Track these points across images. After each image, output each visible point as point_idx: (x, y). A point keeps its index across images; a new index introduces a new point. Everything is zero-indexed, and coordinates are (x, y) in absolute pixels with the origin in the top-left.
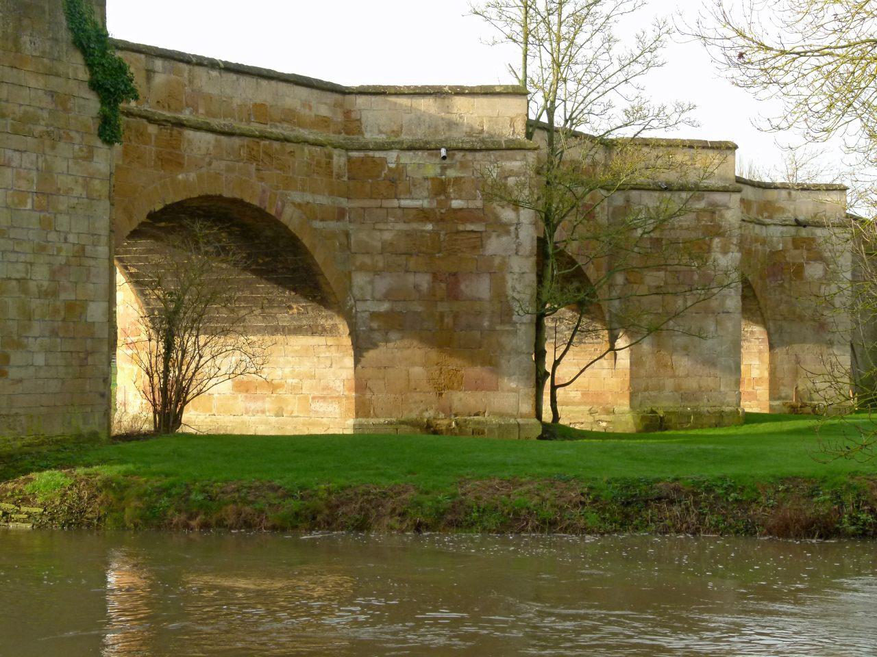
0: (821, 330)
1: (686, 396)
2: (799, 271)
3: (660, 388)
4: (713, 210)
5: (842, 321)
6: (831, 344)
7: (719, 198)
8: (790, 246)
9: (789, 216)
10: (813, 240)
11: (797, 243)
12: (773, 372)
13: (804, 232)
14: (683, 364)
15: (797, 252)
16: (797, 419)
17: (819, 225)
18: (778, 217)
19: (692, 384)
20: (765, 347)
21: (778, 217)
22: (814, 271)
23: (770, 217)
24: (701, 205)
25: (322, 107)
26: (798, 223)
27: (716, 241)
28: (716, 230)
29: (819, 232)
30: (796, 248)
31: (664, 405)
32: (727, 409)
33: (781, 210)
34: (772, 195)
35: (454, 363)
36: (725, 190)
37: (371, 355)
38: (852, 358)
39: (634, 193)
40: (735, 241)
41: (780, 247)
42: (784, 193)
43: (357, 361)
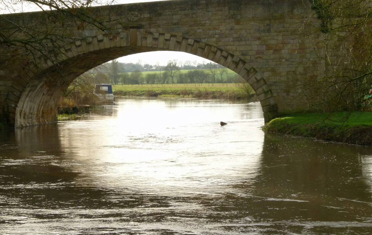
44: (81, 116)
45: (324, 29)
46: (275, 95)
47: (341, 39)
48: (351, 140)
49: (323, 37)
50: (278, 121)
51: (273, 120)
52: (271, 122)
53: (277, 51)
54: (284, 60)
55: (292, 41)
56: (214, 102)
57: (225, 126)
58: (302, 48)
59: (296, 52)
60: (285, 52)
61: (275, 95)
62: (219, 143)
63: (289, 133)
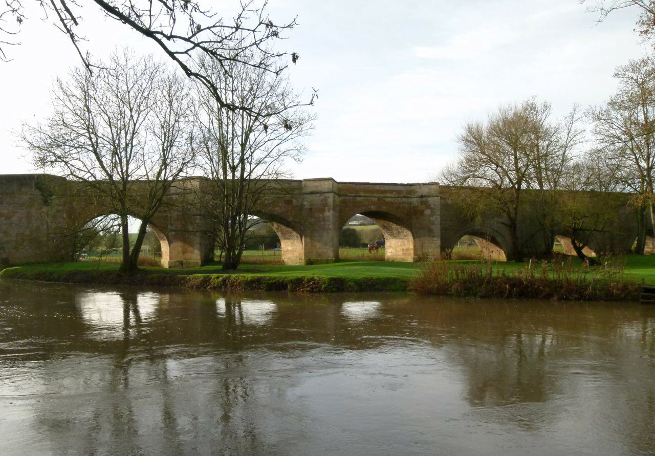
0: (430, 232)
1: (320, 255)
2: (422, 213)
3: (312, 252)
4: (325, 200)
5: (437, 228)
6: (434, 237)
7: (327, 195)
8: (420, 204)
9: (420, 194)
10: (427, 202)
11: (422, 203)
12: (415, 246)
13: (424, 199)
14: (318, 245)
15: (422, 206)
16: (380, 265)
17: (429, 196)
18: (416, 195)
19: (320, 251)
20: (412, 238)
21: (416, 195)
22: (428, 212)
23: (414, 195)
24: (322, 197)
25: (296, 184)
26: (422, 196)
27: (327, 208)
28: (326, 205)
29: (429, 199)
30: (422, 205)
31: (313, 258)
32: (330, 258)
33: (417, 192)
34: (413, 188)
35: (186, 246)
36: (328, 192)
37: (172, 245)
38: (85, 272)
39: (305, 195)
40: (331, 207)
41: (416, 205)
42: (418, 187)
43: (169, 246)
44: (651, 203)
45: (46, 202)
46: (7, 250)
47: (58, 211)
48: (66, 280)
49: (45, 209)
50: (9, 270)
51: (5, 269)
52: (3, 271)
53: (8, 218)
54: (14, 225)
55: (20, 211)
56: (637, 283)
57: (298, 54)
58: (29, 217)
59: (24, 219)
60: (15, 219)
61: (7, 250)
62: (265, 5)
63: (18, 278)
